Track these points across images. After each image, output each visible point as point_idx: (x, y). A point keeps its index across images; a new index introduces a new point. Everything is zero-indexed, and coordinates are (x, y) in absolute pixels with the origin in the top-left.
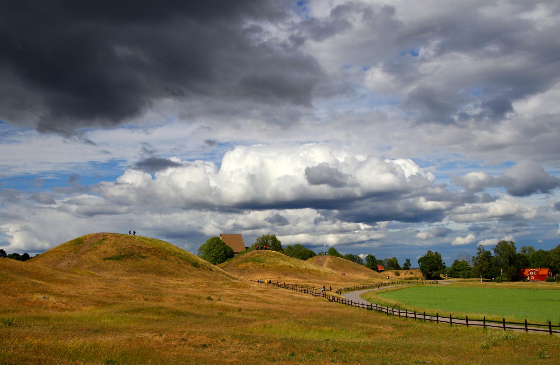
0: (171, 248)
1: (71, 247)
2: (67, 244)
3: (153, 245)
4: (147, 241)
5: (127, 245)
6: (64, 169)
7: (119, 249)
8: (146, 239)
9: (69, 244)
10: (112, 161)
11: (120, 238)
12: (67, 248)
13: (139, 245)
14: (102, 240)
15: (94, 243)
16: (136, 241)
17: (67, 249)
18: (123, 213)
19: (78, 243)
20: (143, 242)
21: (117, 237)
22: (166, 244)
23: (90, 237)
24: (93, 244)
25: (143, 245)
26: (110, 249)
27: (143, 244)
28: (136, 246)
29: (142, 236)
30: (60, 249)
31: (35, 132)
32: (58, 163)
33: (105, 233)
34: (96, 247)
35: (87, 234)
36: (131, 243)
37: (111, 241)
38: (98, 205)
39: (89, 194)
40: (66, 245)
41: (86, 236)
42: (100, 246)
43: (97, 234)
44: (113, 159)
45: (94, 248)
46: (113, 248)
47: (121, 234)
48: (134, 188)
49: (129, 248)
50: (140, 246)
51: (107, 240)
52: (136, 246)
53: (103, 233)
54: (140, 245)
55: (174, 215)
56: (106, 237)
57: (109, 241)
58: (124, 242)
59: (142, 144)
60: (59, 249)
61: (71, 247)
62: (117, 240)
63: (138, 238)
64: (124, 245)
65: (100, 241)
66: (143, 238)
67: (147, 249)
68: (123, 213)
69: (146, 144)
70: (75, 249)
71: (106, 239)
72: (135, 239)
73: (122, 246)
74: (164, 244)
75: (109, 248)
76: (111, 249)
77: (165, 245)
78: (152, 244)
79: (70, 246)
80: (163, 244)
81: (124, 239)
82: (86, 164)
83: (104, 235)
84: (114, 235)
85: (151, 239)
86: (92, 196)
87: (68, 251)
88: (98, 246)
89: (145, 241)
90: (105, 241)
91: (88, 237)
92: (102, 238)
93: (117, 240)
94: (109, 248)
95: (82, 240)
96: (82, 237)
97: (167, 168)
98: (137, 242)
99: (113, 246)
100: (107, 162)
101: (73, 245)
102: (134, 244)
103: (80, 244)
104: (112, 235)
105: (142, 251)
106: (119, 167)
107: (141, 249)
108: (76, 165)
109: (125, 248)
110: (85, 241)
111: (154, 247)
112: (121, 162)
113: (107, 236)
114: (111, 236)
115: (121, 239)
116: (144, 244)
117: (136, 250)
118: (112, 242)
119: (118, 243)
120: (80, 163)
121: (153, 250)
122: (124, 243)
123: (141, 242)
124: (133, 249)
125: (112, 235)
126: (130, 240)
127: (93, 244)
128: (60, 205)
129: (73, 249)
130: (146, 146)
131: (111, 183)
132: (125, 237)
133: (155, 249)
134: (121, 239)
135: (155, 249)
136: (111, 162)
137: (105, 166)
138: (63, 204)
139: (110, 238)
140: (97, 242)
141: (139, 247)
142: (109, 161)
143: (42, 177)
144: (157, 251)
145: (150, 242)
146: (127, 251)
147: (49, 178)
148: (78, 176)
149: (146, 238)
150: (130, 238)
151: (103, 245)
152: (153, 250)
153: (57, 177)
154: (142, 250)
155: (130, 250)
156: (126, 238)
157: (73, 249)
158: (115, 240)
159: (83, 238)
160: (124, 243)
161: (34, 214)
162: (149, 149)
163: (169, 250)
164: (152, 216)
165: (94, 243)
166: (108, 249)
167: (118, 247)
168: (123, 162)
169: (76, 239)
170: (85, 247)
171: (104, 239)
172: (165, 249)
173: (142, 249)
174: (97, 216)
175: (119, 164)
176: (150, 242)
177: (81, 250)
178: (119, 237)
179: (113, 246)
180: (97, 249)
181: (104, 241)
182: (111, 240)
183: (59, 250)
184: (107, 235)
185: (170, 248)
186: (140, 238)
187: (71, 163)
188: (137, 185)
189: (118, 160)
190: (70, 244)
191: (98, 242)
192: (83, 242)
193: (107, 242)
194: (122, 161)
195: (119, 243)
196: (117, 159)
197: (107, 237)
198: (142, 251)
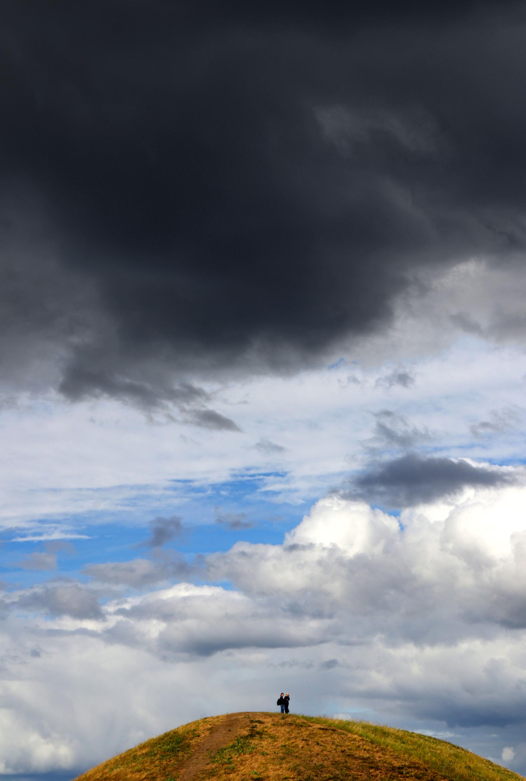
0: (472, 766)
1: (152, 762)
2: (139, 753)
3: (410, 755)
4: (389, 741)
5: (325, 753)
6: (103, 506)
7: (302, 769)
8: (385, 734)
9: (144, 751)
10: (242, 476)
11: (303, 729)
12: (140, 767)
13: (367, 755)
14: (246, 737)
15: (223, 750)
16: (355, 740)
17: (139, 771)
18: (310, 642)
19: (173, 750)
20: (379, 744)
21: (293, 727)
22: (452, 752)
23: (209, 726)
24: (220, 751)
25: (379, 754)
26: (275, 770)
27: (377, 752)
28: (356, 758)
29: (373, 723)
30: (119, 770)
31: (53, 394)
32: (80, 489)
33: (254, 714)
34: (231, 763)
35: (197, 717)
36: (340, 749)
37: (275, 741)
38: (228, 617)
39: (198, 584)
40: (135, 757)
41: (196, 723)
42: (243, 757)
43: (229, 716)
44: (248, 469)
45: (223, 764)
46: (284, 766)
47: (303, 717)
48: (341, 562)
49: (335, 764)
50: (369, 758)
51: (261, 739)
52: (356, 758)
53: (247, 715)
54: (368, 755)
55: (464, 646)
56: (259, 728)
57: (270, 740)
58: (318, 744)
59: (376, 415)
60: (115, 771)
61: (152, 762)
62: (296, 738)
63: (361, 731)
64: (318, 754)
65: (242, 740)
66: (375, 730)
67: (393, 769)
68: (310, 642)
69: (388, 413)
70: (164, 769)
71: (258, 733)
72: (350, 735)
73: (311, 757)
74: (446, 751)
75: (271, 767)
76: (278, 767)
77: (450, 755)
78: (406, 751)
79: (148, 759)
80: (441, 750)
81: (315, 735)
82: (166, 489)
83: (252, 722)
84: (282, 721)
85: (401, 734)
86: (206, 591)
87: (144, 776)
88: (235, 757)
89: (382, 740)
90: (256, 742)
91: (201, 728)
92: (245, 733)
93: (296, 738)
94: (271, 767)
95: (184, 738)
96: (183, 727)
97: (461, 489)
98: (357, 744)
99: (283, 759)
100: (230, 479)
101: (158, 756)
102: (348, 752)
103: (180, 754)
104: (276, 719)
105: (377, 776)
106: (267, 493)
107: (372, 768)
108: (134, 493)
109: (322, 766)
110: (193, 742)
111: (415, 763)
112: (271, 478)
113: (260, 722)
114: (274, 725)
115: (308, 732)
116: (382, 749)
117: (358, 770)
118: (280, 743)
119: (297, 746)
120: (146, 487)
121: (414, 772)
122: (317, 749)
123: (372, 742)
124: (348, 768)
125: (276, 719)
126: (335, 736)
127: (220, 751)
128: (113, 621)
129: (158, 768)
130: (387, 422)
131: (273, 550)
132: (319, 726)
133: (418, 768)
134: (305, 733)
135: (418, 768)
136: (240, 478)
137: (223, 493)
138: (120, 618)
139: (272, 731)
140: (231, 744)
141: (364, 759)
142: (234, 476)
143: (35, 534)
144: (423, 774)
145: (398, 745)
146: (328, 775)
147: (56, 536)
148: (176, 523)
149: (386, 730)
150: (333, 730)
151: (251, 753)
152: (414, 772)
153: (80, 533)
154: (378, 772)
155: (337, 772)
156: (320, 729)
157: (158, 768)
158: (289, 739)
159: (188, 733)
160: (317, 749)
161: (36, 654)
162: (399, 429)
163: (465, 772)
164: (391, 651)
165: (223, 750)
166: (267, 769)
167: (298, 762)
168: (279, 478)
169: (166, 735)
170: (195, 761)
171: (252, 736)
172: (453, 770)
173: (377, 768)
174: (219, 657)
175: (265, 485)
176: (398, 745)
177: (182, 771)
178: (300, 726)
179: (283, 759)
180: (233, 770)
181: (255, 742)
182: (274, 738)
183: (115, 775)
184: (261, 719)
185: (469, 768)
186: (366, 730)
187: (120, 488)
188: (351, 553)
189: (263, 471)
190: (146, 754)
191: (233, 746)
192: (188, 746)
193: (264, 743)
194: (277, 474)
195: (301, 746)
196: (258, 468)
197: (262, 726)
198: (377, 776)
